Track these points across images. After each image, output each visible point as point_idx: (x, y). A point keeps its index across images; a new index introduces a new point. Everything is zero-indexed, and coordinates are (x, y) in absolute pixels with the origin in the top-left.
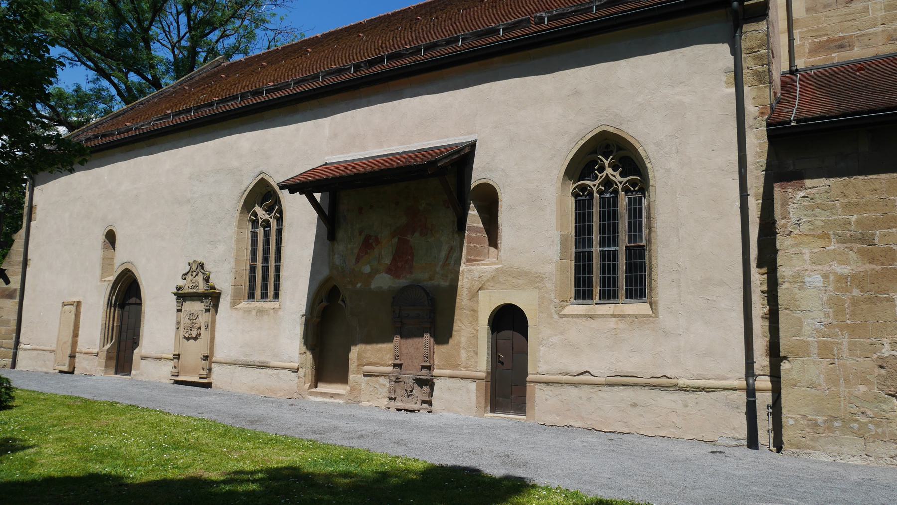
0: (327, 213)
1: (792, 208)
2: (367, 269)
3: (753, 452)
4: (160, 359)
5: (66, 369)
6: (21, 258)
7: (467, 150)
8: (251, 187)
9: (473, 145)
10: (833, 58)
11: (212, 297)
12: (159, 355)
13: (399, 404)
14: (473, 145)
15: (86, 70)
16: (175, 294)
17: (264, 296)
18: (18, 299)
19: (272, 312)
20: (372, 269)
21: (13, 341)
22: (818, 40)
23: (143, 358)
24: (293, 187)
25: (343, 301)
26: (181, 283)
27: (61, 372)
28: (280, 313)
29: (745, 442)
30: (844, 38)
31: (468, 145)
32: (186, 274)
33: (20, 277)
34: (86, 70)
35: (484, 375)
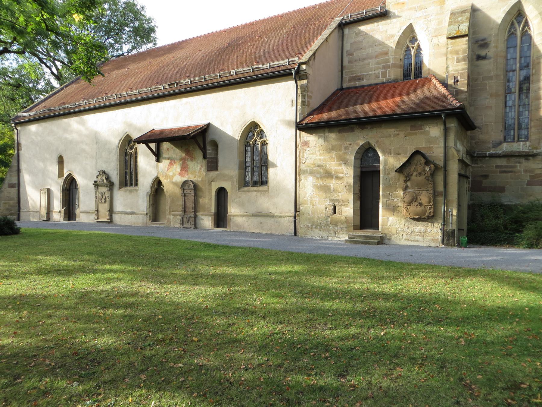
0: (155, 151)
1: (305, 154)
2: (171, 174)
3: (295, 237)
4: (89, 213)
5: (45, 219)
6: (17, 169)
7: (205, 127)
8: (123, 138)
9: (411, 24)
10: (356, 84)
11: (110, 185)
12: (89, 211)
13: (185, 226)
14: (411, 24)
15: (143, 8)
16: (93, 184)
17: (131, 185)
18: (17, 188)
19: (135, 191)
20: (173, 174)
21: (17, 208)
22: (352, 76)
23: (81, 212)
24: (139, 141)
25: (163, 186)
26: (96, 179)
27: (43, 220)
28: (139, 191)
29: (293, 234)
30: (361, 75)
31: (205, 125)
32: (98, 176)
33: (17, 178)
34: (143, 8)
35: (213, 214)
